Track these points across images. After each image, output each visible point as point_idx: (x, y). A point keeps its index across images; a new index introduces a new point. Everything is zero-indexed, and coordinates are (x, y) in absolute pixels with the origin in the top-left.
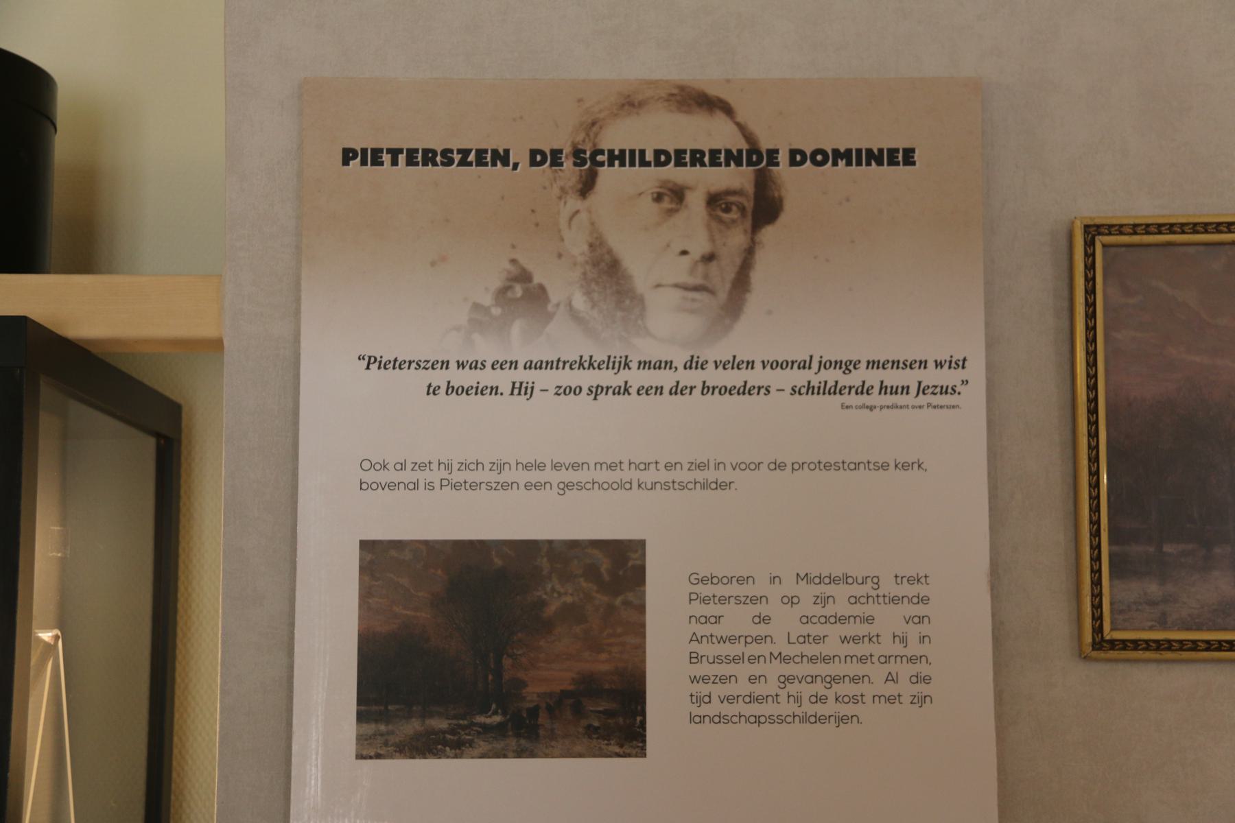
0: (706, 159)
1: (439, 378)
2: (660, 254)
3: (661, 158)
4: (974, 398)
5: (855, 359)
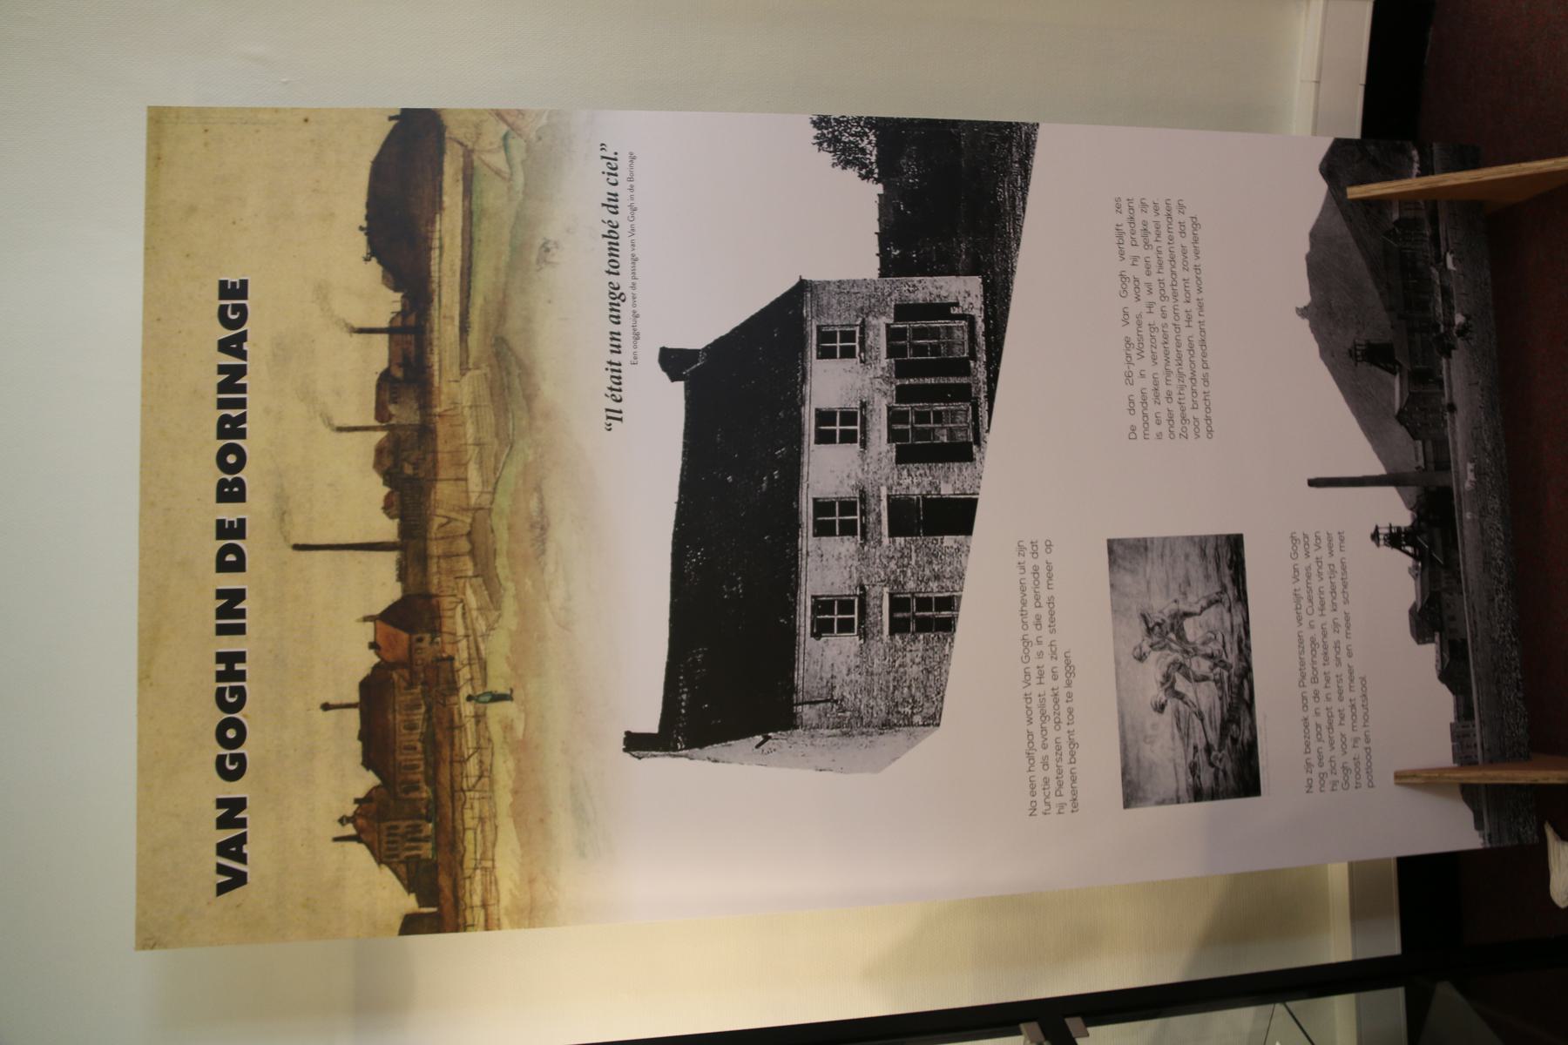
0: (234, 413)
5: (608, 289)
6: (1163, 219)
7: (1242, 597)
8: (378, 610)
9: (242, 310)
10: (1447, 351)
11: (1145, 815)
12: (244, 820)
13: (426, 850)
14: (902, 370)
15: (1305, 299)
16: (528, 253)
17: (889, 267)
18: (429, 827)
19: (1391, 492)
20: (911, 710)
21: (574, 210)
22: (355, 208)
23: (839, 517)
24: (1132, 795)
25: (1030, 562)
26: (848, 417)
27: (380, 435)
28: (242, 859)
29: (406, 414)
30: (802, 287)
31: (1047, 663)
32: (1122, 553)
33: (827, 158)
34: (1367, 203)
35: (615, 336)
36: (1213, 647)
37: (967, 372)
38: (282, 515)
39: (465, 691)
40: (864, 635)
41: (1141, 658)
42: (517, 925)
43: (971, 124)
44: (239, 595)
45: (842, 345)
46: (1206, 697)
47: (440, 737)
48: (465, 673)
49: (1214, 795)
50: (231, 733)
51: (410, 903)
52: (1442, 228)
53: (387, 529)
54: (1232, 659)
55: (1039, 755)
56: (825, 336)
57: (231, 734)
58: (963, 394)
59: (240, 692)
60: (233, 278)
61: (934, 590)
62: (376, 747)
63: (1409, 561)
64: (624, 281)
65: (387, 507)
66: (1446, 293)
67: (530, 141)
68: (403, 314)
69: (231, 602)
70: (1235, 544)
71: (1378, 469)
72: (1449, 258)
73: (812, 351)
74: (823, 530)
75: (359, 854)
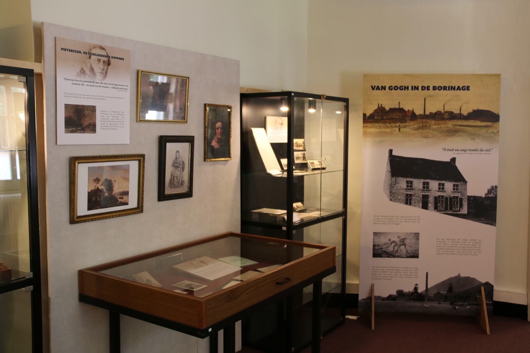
1: (73, 82)
2: (98, 68)
3: (98, 55)
4: (129, 90)
6: (477, 249)
7: (408, 257)
8: (414, 111)
9: (465, 90)
10: (451, 304)
11: (372, 236)
13: (376, 118)
14: (451, 198)
15: (462, 275)
16: (473, 136)
17: (469, 197)
18: (379, 118)
19: (424, 289)
20: (393, 196)
21: (481, 144)
22: (482, 107)
23: (426, 186)
24: (375, 234)
25: (416, 218)
26: (443, 189)
27: (443, 112)
29: (446, 116)
30: (466, 182)
31: (399, 220)
32: (417, 236)
33: (489, 188)
34: (480, 291)
35: (458, 150)
36: (399, 250)
37: (450, 210)
38: (430, 96)
39: (401, 124)
40: (406, 189)
41: (398, 237)
42: (363, 131)
43: (496, 214)
44: (418, 89)
45: (456, 188)
46: (391, 249)
47: (393, 120)
48: (403, 124)
49: (374, 249)
50: (396, 88)
51: (368, 115)
52: (475, 306)
53: (427, 113)
54: (397, 254)
55: (384, 218)
56: (457, 186)
58: (446, 209)
59: (402, 89)
60: (470, 88)
61: (413, 201)
62: (393, 110)
63: (411, 291)
64: (468, 152)
65: (431, 113)
66: (462, 305)
67: (494, 137)
68: (463, 116)
69: (416, 88)
70: (417, 257)
71: (429, 287)
72: (469, 307)
73: (455, 183)
74: (424, 183)
75: (376, 107)
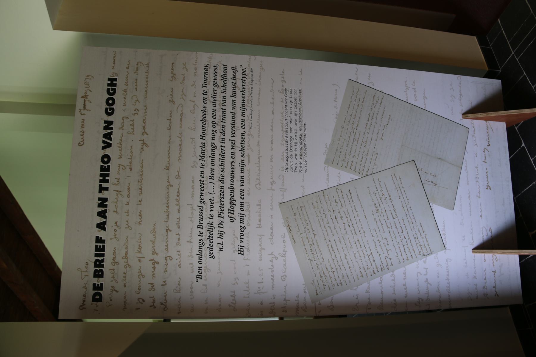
0: (100, 259)
12: (107, 205)
28: (111, 139)
57: (110, 102)
59: (115, 90)
